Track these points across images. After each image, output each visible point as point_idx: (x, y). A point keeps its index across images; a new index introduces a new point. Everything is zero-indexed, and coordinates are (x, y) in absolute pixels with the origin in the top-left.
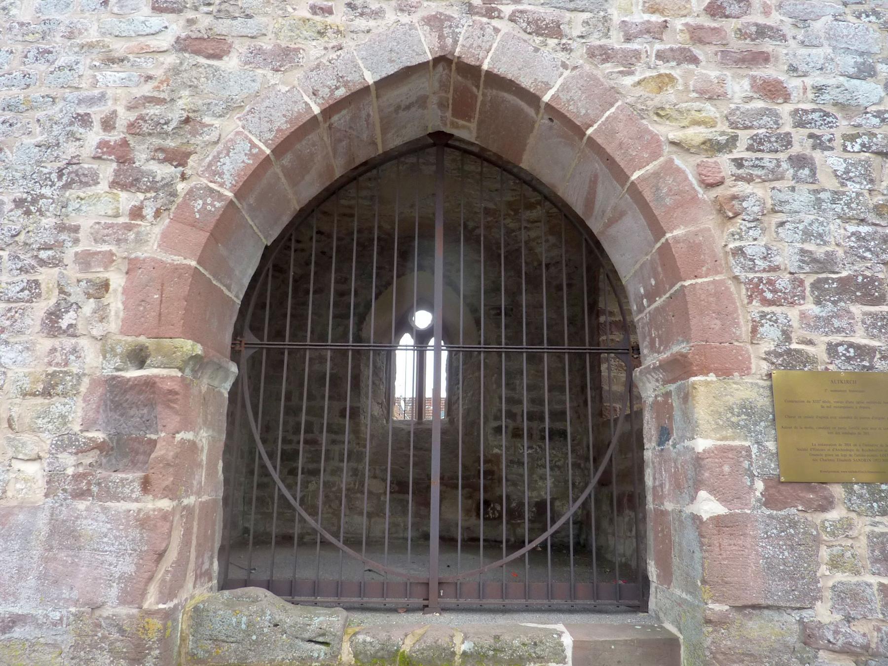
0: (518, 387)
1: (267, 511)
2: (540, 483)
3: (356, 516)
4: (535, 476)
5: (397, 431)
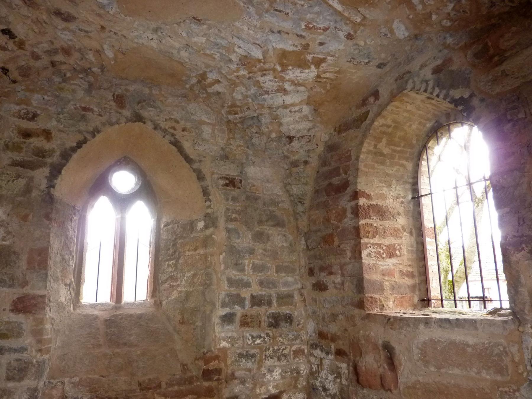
0: (246, 268)
2: (268, 377)
4: (263, 369)
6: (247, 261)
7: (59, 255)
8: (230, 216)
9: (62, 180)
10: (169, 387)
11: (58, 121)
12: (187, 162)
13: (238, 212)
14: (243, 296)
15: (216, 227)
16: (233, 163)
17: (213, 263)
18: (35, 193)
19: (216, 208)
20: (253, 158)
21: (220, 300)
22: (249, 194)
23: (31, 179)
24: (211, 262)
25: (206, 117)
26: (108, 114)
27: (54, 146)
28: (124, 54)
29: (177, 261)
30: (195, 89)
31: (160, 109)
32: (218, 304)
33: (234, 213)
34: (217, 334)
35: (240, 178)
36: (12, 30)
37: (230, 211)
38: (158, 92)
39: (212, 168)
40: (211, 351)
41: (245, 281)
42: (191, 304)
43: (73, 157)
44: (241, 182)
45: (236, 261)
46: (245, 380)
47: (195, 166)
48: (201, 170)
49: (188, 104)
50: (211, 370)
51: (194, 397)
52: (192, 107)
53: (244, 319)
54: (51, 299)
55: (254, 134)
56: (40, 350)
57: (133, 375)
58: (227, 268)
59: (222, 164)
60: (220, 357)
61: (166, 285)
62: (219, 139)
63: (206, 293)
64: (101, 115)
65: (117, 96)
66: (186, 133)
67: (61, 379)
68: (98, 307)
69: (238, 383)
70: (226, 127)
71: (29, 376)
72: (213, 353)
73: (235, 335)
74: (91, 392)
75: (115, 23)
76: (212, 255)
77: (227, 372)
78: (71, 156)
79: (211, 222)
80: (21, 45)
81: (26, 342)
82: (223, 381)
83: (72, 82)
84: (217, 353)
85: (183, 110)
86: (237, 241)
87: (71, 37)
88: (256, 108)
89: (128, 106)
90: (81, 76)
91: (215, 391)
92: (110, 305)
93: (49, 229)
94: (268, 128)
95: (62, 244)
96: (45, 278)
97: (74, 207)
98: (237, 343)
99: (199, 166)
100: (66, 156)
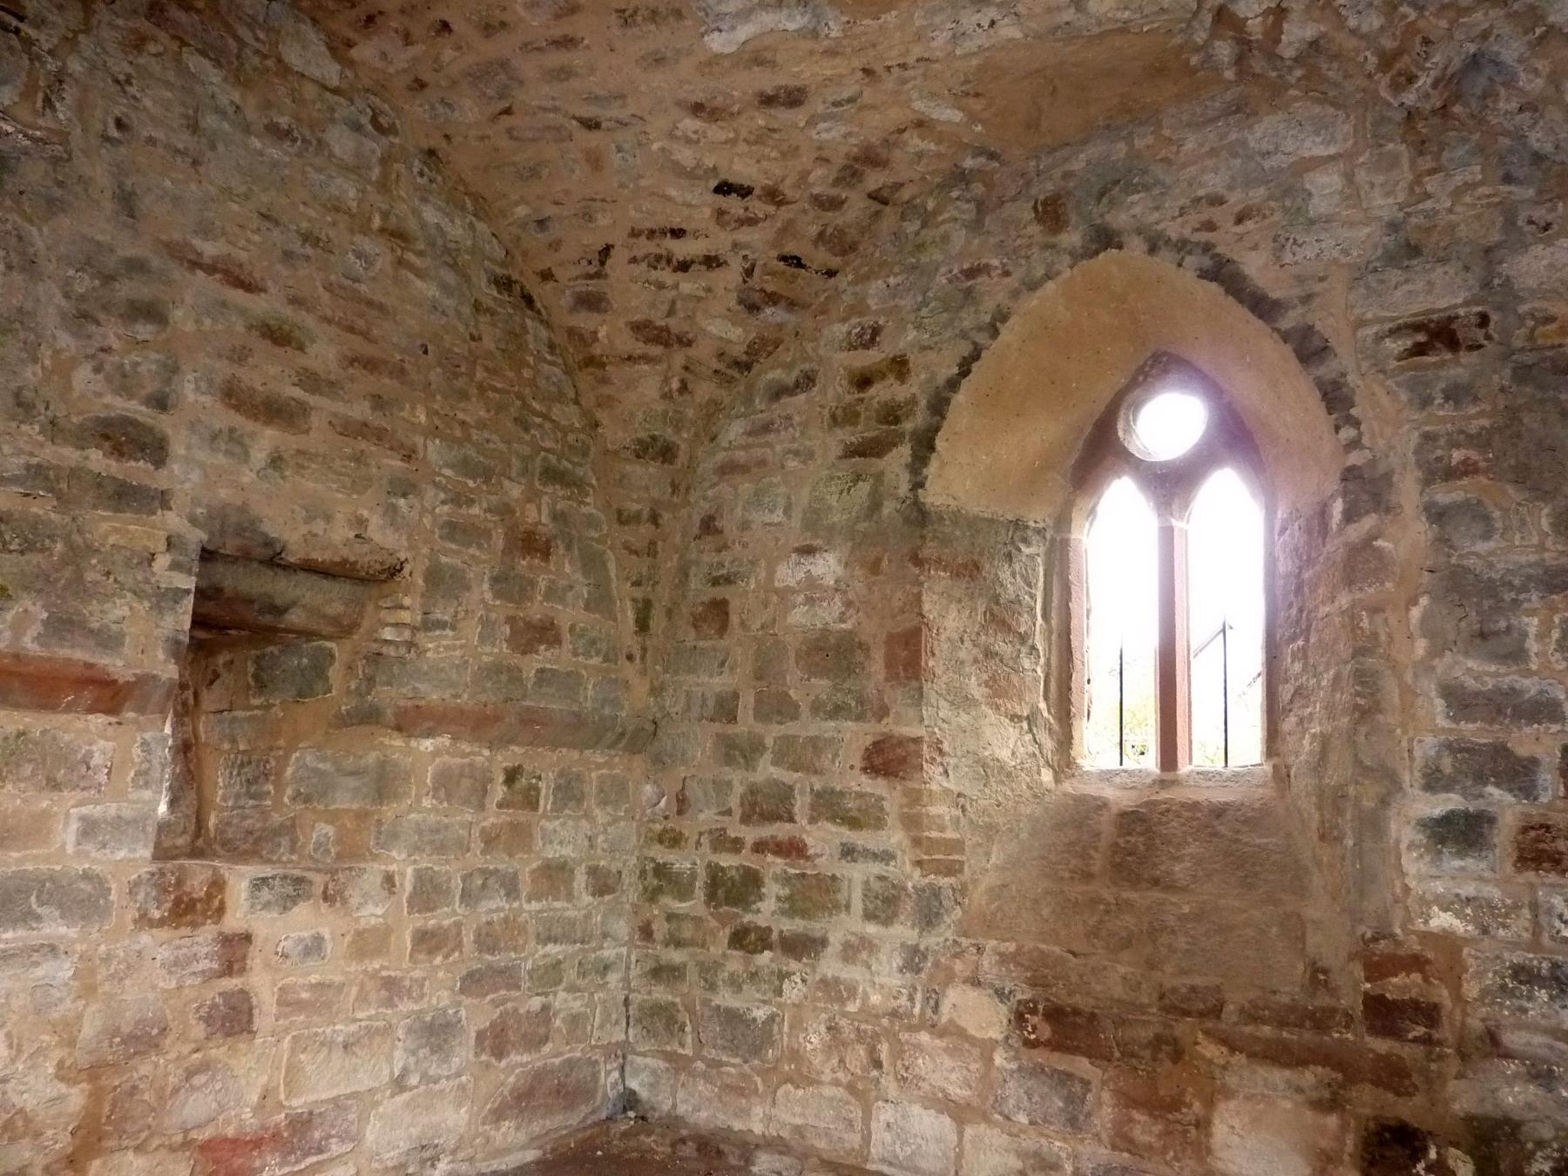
0: (1533, 646)
1: (680, 1051)
3: (916, 1109)
5: (1084, 811)
6: (1535, 621)
7: (968, 644)
8: (1438, 459)
9: (943, 465)
10: (1246, 1024)
11: (919, 327)
12: (1260, 317)
13: (1473, 440)
14: (1523, 751)
15: (1388, 510)
16: (1442, 261)
17: (1383, 638)
18: (888, 508)
19: (1381, 442)
20: (1540, 214)
21: (1419, 763)
22: (1529, 358)
23: (879, 477)
24: (1375, 635)
25: (1318, 140)
26: (1023, 262)
27: (914, 389)
28: (977, 95)
29: (1307, 640)
30: (1258, 70)
31: (1163, 185)
32: (1410, 779)
33: (1458, 446)
34: (1412, 884)
35: (1480, 309)
36: (731, 180)
37: (1442, 442)
38: (1150, 140)
39: (1353, 307)
40: (1393, 936)
41: (1527, 696)
42: (1333, 778)
43: (953, 402)
44: (1484, 320)
45: (1481, 622)
46: (1551, 1071)
47: (1288, 321)
48: (1311, 328)
49: (1250, 127)
50: (1394, 1002)
51: (1334, 1075)
52: (1260, 133)
53: (1538, 840)
54: (946, 747)
55: (1518, 118)
56: (919, 863)
57: (1152, 965)
58: (1435, 652)
59: (1394, 281)
60: (1428, 962)
61: (1292, 719)
62: (1377, 192)
63: (1361, 739)
64: (1007, 274)
65: (1045, 203)
66: (1249, 225)
67: (981, 941)
68: (1117, 780)
69: (1516, 1076)
70: (1404, 141)
71: (902, 918)
72: (1398, 943)
73: (1494, 893)
74: (1033, 983)
75: (874, 46)
76: (1375, 610)
77: (1463, 1023)
78: (947, 401)
79: (1365, 497)
80: (774, 196)
81: (893, 840)
82: (1449, 1051)
83: (940, 219)
84: (1417, 948)
85: (1235, 155)
86: (1482, 547)
87: (843, 130)
88: (1444, 24)
89: (1074, 218)
90: (954, 194)
91: (1416, 1079)
92: (1148, 774)
93: (921, 584)
94: (1536, 72)
95: (980, 618)
96: (919, 698)
97: (1018, 525)
98: (1505, 926)
99: (1303, 315)
100: (939, 407)
